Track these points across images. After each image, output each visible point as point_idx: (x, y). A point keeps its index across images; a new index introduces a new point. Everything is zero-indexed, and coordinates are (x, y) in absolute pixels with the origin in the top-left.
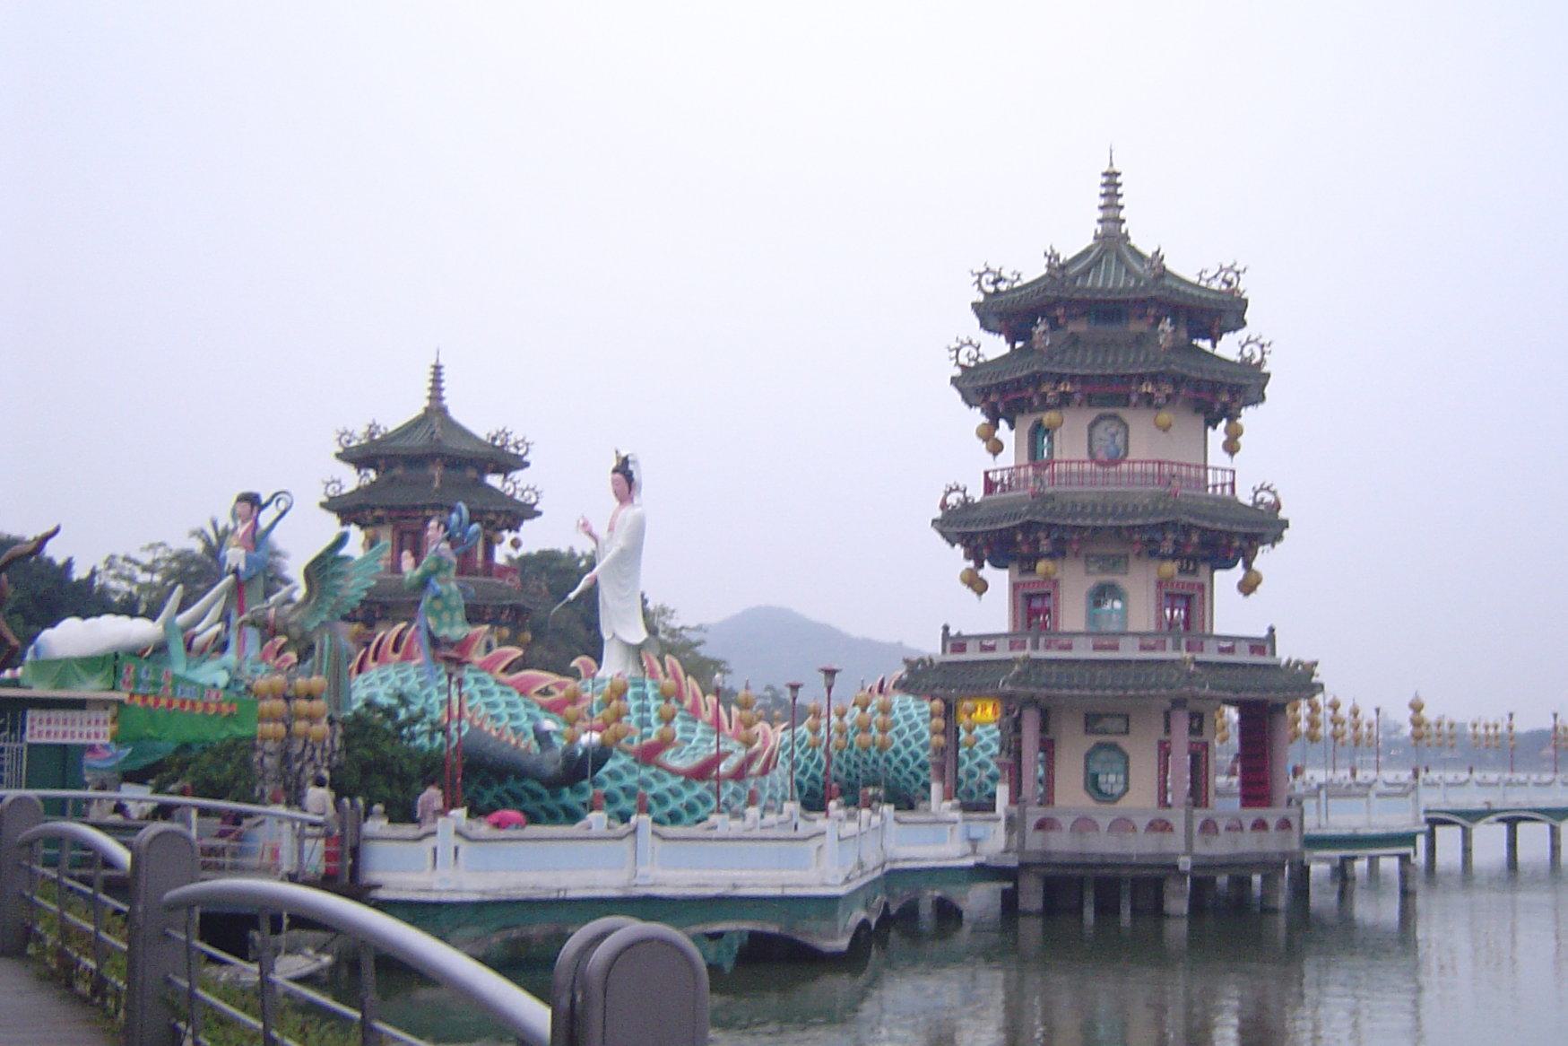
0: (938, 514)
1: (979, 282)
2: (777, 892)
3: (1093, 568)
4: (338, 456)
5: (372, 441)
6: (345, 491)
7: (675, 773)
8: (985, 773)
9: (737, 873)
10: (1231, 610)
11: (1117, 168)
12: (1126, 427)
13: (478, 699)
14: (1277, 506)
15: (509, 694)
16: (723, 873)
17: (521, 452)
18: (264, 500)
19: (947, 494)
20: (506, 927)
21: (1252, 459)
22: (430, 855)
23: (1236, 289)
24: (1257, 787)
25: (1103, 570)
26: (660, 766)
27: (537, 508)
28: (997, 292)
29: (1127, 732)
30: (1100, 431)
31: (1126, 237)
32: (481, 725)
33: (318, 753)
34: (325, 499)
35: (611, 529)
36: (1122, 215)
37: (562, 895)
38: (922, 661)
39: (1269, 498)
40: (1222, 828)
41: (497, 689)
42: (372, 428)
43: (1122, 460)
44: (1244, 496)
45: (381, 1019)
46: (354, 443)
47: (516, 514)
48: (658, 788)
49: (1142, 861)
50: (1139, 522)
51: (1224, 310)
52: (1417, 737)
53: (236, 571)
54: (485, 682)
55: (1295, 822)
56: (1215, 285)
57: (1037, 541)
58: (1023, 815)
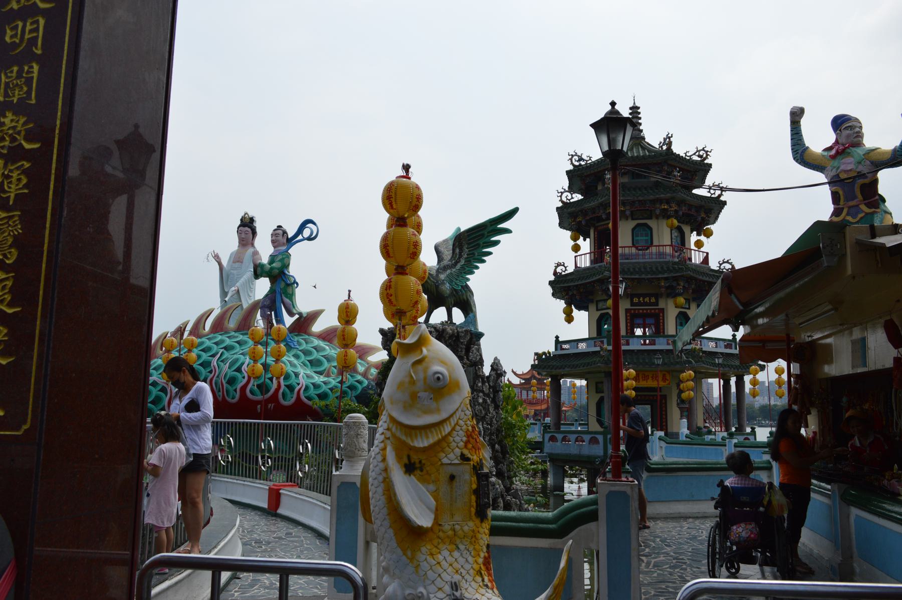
0: (552, 278)
1: (571, 159)
11: (637, 104)
12: (651, 229)
19: (556, 267)
28: (580, 165)
31: (644, 138)
38: (544, 353)
39: (728, 266)
45: (37, 149)
50: (666, 275)
56: (695, 158)
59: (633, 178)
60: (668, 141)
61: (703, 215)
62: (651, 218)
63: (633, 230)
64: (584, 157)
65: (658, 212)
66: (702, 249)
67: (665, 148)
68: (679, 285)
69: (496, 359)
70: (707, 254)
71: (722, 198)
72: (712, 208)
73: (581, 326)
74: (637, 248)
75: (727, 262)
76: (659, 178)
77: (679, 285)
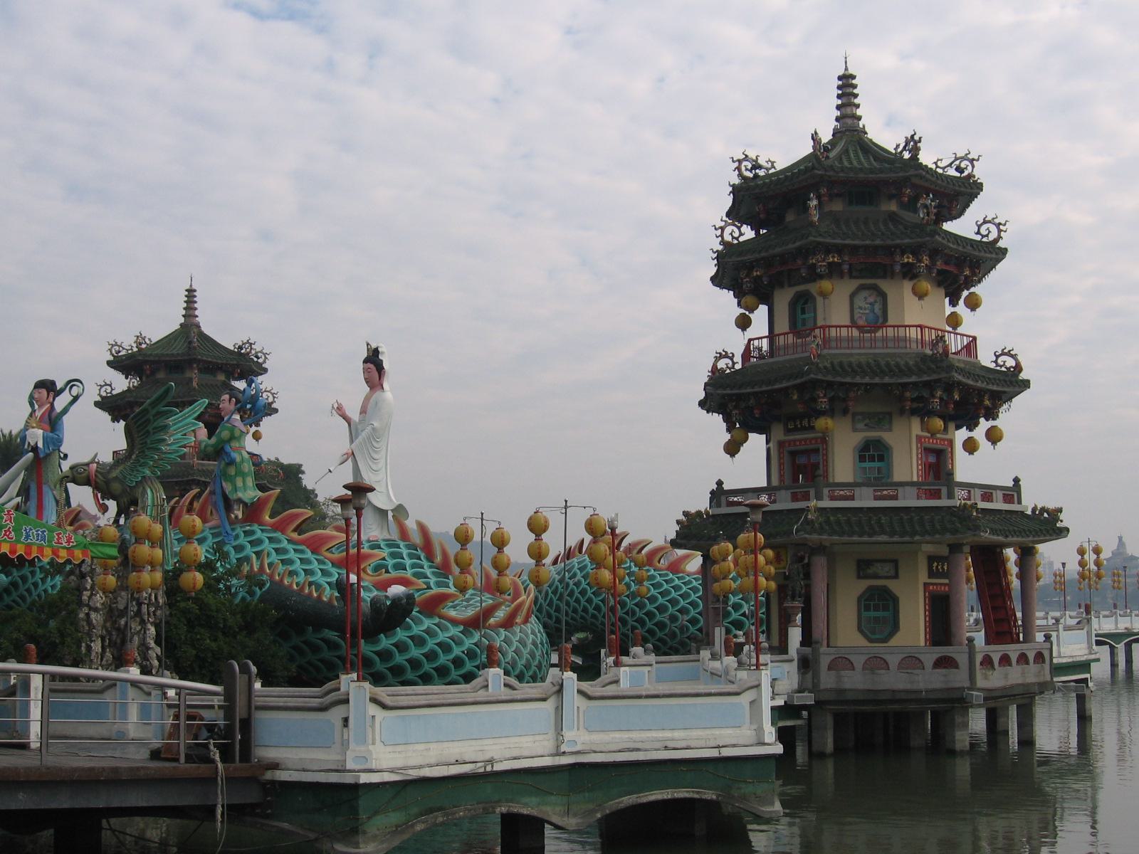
1: (738, 168)
2: (714, 753)
3: (860, 426)
4: (109, 363)
5: (140, 350)
6: (114, 392)
7: (455, 622)
8: (686, 618)
9: (668, 734)
10: (978, 465)
12: (883, 296)
13: (274, 557)
14: (1018, 368)
15: (301, 552)
16: (654, 734)
17: (260, 361)
18: (59, 385)
19: (717, 359)
20: (431, 811)
21: (991, 324)
22: (339, 723)
23: (970, 176)
24: (1001, 626)
25: (869, 427)
26: (441, 617)
27: (274, 406)
28: (756, 176)
29: (896, 576)
30: (859, 302)
32: (282, 580)
33: (144, 608)
34: (98, 399)
35: (363, 411)
36: (859, 112)
37: (489, 769)
39: (1010, 363)
40: (1014, 660)
41: (290, 547)
42: (140, 339)
43: (884, 324)
44: (985, 358)
46: (123, 353)
47: (256, 410)
48: (442, 636)
49: (932, 696)
50: (913, 379)
51: (959, 191)
52: (1082, 576)
53: (35, 449)
54: (279, 541)
55: (1046, 654)
56: (952, 172)
57: (814, 400)
58: (816, 653)
59: (850, 203)
60: (913, 144)
61: (967, 273)
62: (884, 277)
63: (852, 296)
64: (762, 161)
65: (898, 268)
66: (959, 330)
67: (907, 155)
68: (933, 396)
69: (344, 487)
70: (975, 339)
71: (1001, 244)
72: (979, 259)
73: (751, 466)
74: (858, 327)
75: (1009, 354)
76: (893, 207)
77: (933, 396)
